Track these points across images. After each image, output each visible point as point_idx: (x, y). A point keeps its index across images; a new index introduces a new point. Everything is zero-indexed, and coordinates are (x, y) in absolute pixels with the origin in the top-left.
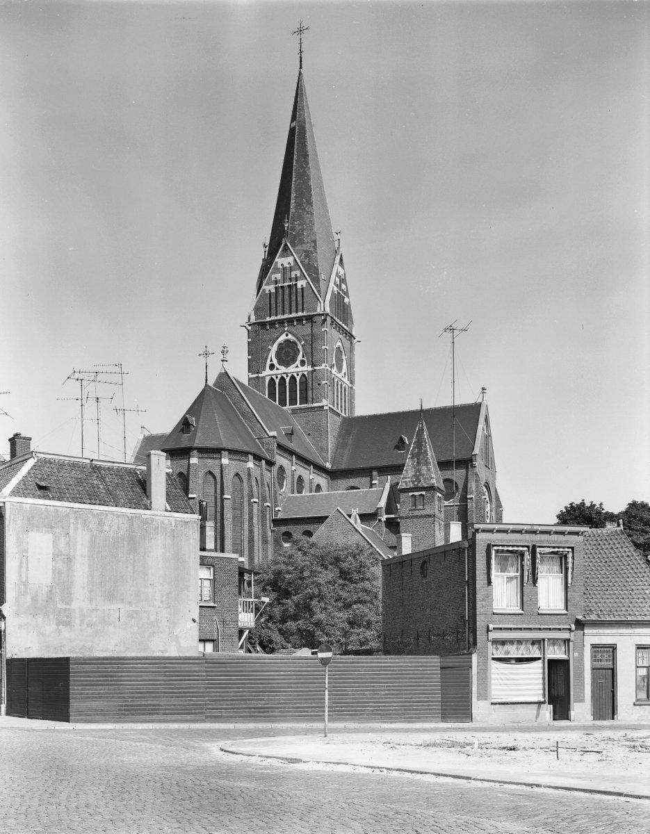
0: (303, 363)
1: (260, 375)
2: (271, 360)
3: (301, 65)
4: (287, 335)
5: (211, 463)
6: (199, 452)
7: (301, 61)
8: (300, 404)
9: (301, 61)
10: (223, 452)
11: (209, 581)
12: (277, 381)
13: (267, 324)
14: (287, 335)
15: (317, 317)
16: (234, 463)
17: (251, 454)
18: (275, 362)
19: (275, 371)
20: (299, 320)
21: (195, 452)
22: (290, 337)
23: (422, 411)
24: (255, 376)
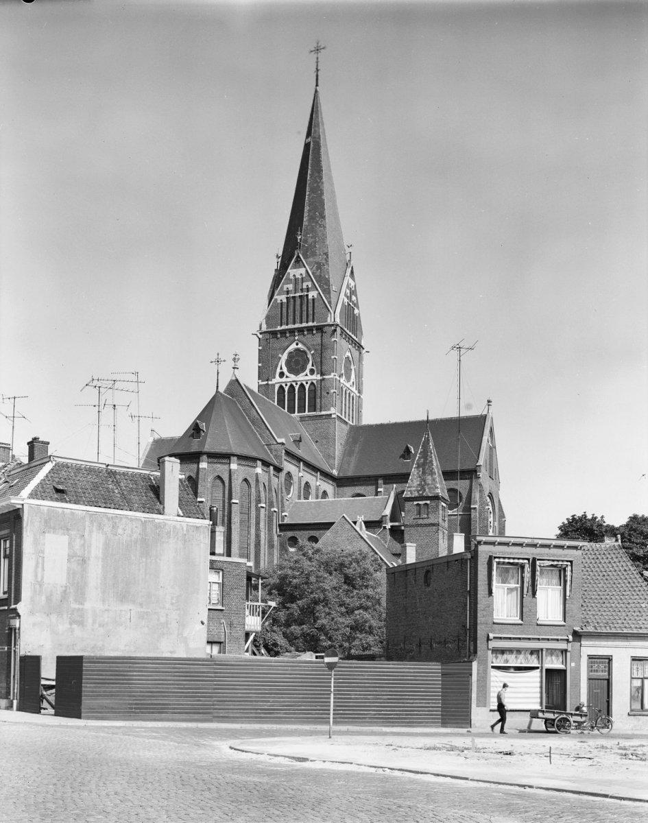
0: (312, 372)
1: (270, 382)
2: (281, 369)
4: (297, 344)
10: (232, 458)
12: (286, 389)
13: (314, 329)
14: (297, 344)
17: (260, 460)
18: (285, 370)
19: (284, 379)
20: (310, 329)
21: (205, 457)
22: (300, 346)
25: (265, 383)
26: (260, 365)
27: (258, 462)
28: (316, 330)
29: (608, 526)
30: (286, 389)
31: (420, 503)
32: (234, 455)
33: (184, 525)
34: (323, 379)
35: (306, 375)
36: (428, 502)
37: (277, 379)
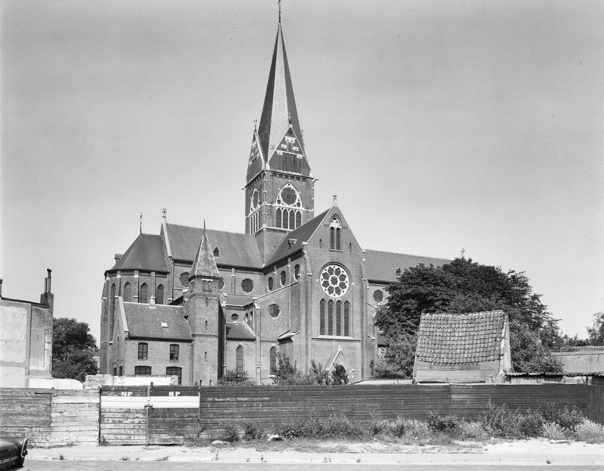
0: (299, 205)
1: (309, 210)
2: (279, 198)
3: (280, 20)
4: (289, 185)
5: (144, 279)
6: (109, 273)
7: (280, 18)
8: (290, 229)
9: (280, 18)
10: (135, 271)
11: (102, 397)
12: (282, 211)
13: (278, 174)
14: (289, 185)
15: (309, 179)
16: (125, 277)
17: (137, 270)
18: (281, 199)
19: (281, 205)
20: (298, 178)
21: (119, 272)
22: (291, 186)
23: (204, 231)
24: (306, 210)
25: (306, 210)
26: (313, 199)
27: (135, 271)
28: (279, 175)
29: (480, 266)
30: (282, 211)
31: (206, 280)
32: (153, 271)
33: (357, 337)
34: (271, 203)
35: (295, 206)
36: (212, 280)
37: (276, 205)
